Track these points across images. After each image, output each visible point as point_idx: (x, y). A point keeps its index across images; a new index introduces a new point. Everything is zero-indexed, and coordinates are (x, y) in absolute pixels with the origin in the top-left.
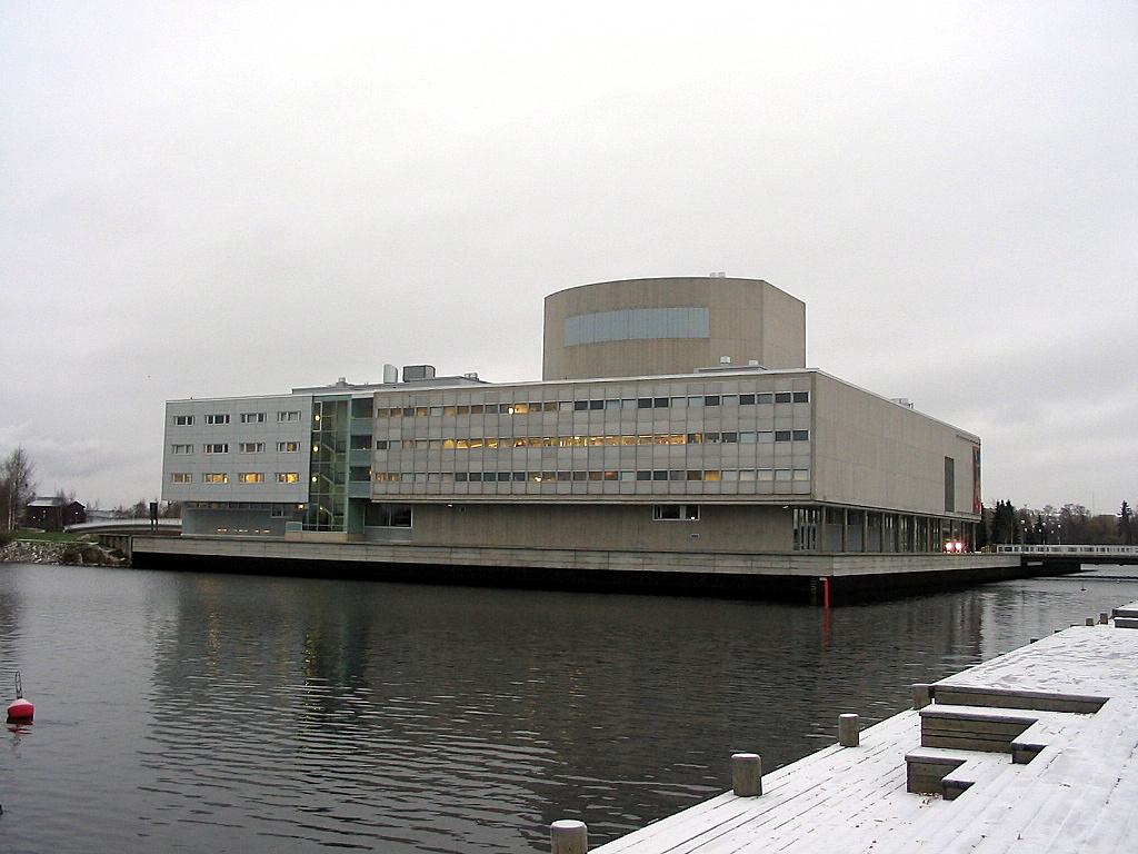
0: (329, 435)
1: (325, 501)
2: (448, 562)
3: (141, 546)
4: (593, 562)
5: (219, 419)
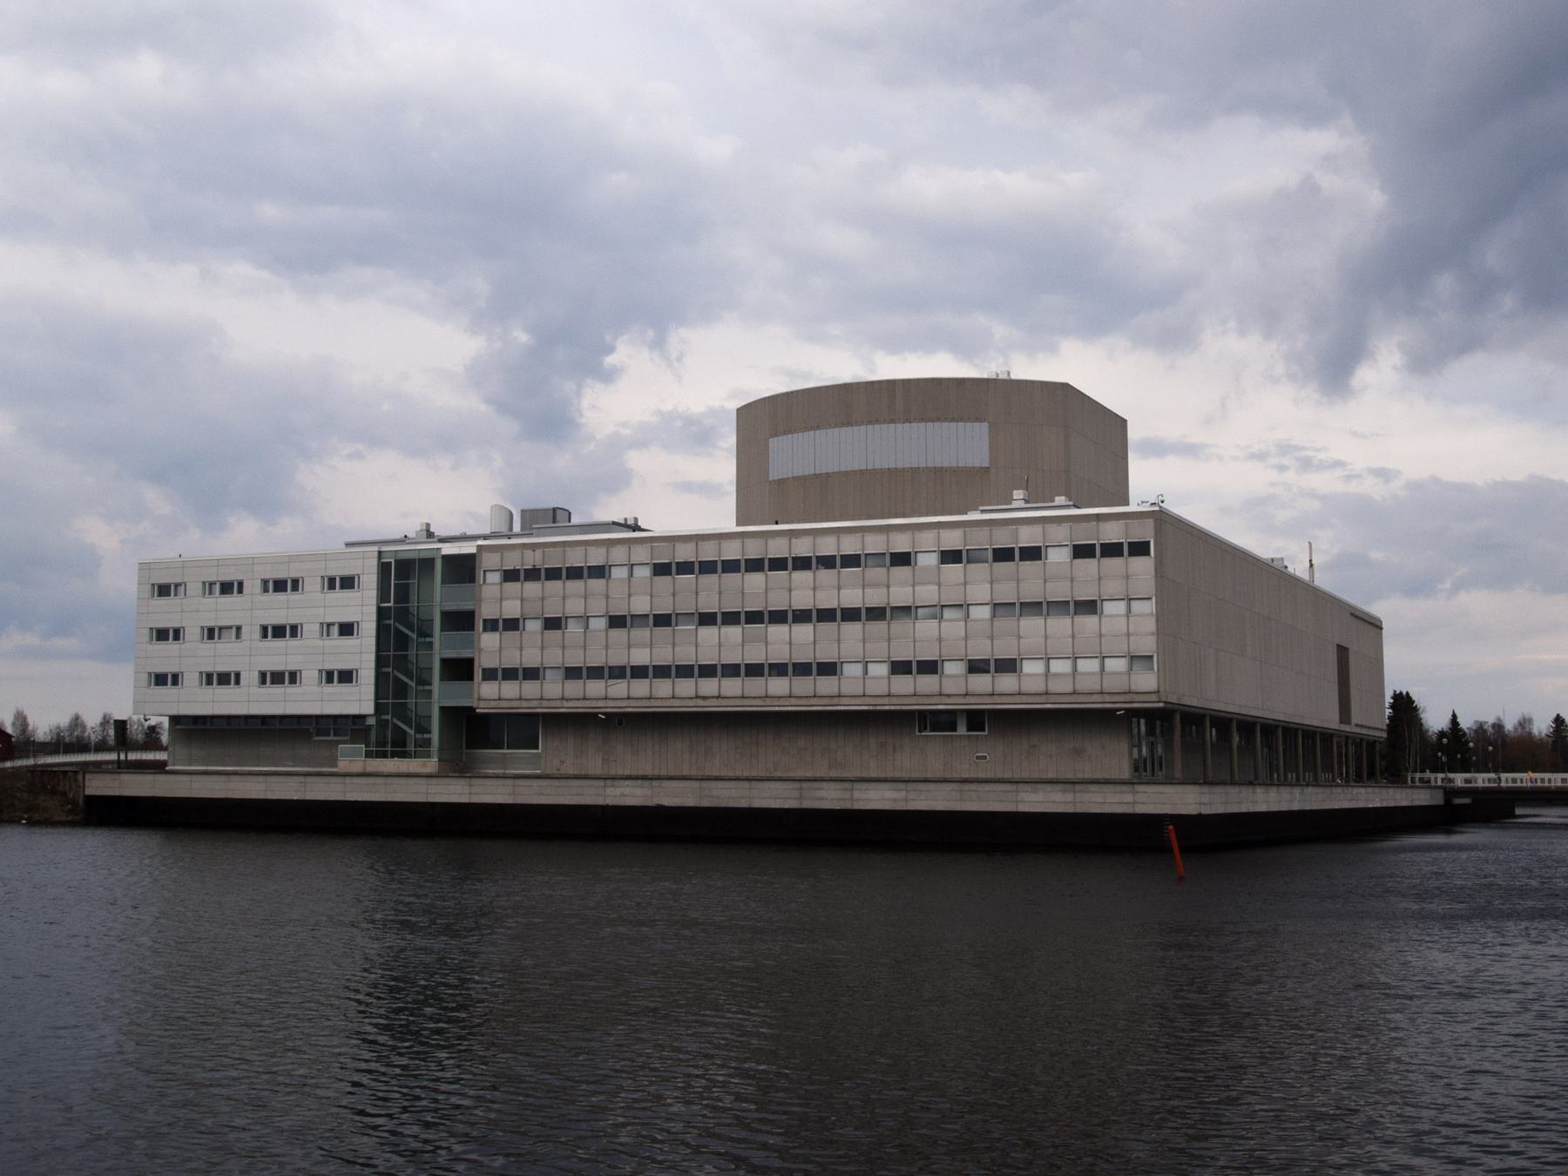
0: (406, 611)
1: (401, 711)
2: (600, 801)
3: (98, 786)
4: (829, 798)
5: (226, 588)
